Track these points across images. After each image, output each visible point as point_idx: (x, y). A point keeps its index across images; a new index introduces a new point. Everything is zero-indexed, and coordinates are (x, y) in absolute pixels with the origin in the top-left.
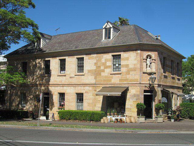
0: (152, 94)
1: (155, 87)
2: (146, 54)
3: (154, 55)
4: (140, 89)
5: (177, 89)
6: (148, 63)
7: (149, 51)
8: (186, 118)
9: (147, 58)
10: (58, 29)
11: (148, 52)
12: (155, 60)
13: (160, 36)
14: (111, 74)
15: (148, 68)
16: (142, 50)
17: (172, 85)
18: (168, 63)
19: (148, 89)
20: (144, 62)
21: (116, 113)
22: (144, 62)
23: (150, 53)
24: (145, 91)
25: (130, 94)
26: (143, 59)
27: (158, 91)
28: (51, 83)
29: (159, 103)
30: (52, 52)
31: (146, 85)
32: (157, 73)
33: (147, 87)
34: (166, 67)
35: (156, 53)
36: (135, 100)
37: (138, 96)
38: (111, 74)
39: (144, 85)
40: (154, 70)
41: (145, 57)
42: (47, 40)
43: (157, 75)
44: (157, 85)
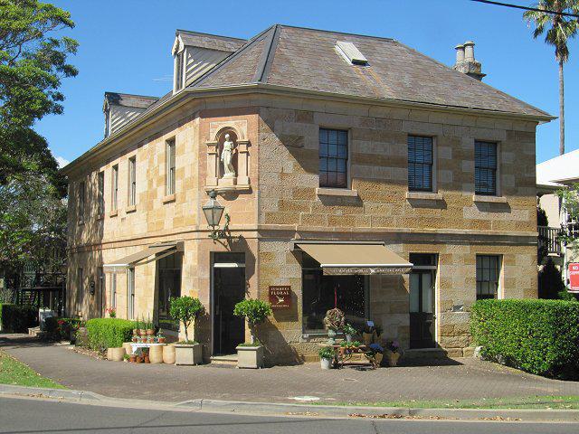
0: (243, 265)
2: (218, 124)
3: (244, 126)
5: (471, 244)
6: (227, 157)
8: (497, 362)
11: (223, 118)
13: (472, 45)
14: (165, 203)
15: (229, 175)
16: (205, 114)
17: (405, 230)
19: (223, 249)
23: (230, 122)
24: (216, 257)
26: (209, 145)
28: (106, 238)
30: (349, 140)
35: (254, 117)
38: (165, 203)
40: (243, 182)
41: (213, 139)
42: (131, 114)
44: (255, 234)
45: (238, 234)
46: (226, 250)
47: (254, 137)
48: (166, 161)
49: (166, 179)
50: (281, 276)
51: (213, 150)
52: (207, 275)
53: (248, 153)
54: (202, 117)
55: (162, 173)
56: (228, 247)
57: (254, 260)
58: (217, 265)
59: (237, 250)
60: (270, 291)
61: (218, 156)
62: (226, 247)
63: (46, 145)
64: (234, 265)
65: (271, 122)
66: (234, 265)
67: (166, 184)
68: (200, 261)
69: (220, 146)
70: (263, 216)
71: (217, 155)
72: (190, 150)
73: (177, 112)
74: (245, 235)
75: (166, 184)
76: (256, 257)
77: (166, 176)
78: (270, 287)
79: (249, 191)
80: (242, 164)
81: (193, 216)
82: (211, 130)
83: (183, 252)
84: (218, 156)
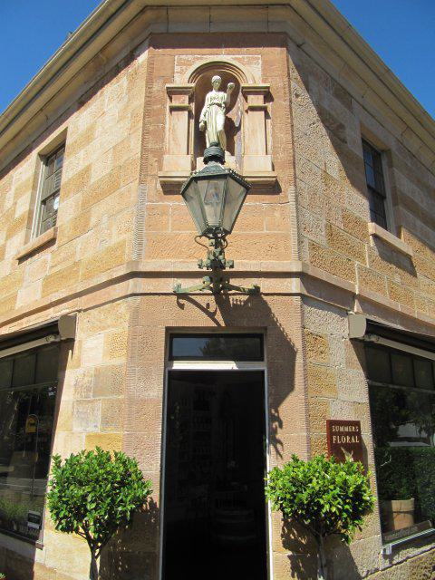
1: (275, 306)
4: (135, 320)
6: (214, 119)
7: (219, 46)
9: (206, 87)
10: (122, 272)
12: (268, 96)
14: (22, 259)
18: (400, 181)
19: (203, 321)
20: (173, 109)
21: (356, 522)
22: (173, 109)
25: (80, 371)
26: (171, 92)
27: (313, 339)
29: (336, 451)
31: (188, 285)
32: (288, 191)
33: (202, 301)
34: (395, 204)
35: (277, 54)
36: (98, 430)
37: (117, 389)
38: (22, 259)
39: (170, 285)
41: (182, 79)
43: (292, 205)
44: (294, 285)
45: (248, 284)
46: (213, 324)
47: (277, 84)
48: (34, 188)
49: (30, 218)
50: (341, 396)
51: (183, 100)
52: (155, 391)
53: (265, 109)
54: (156, 47)
55: (22, 209)
56: (219, 317)
57: (293, 353)
58: (179, 366)
59: (245, 324)
60: (330, 434)
61: (195, 116)
62: (212, 315)
63: (284, 543)
64: (230, 366)
65: (308, 71)
66: (230, 366)
67: (29, 228)
68: (135, 346)
69: (198, 98)
70: (306, 245)
71: (190, 112)
72: (141, 70)
73: (81, 78)
74: (266, 285)
75: (29, 228)
76: (298, 345)
78: (331, 423)
79: (272, 188)
80: (254, 132)
81: (121, 245)
82: (177, 69)
83: (73, 340)
84: (195, 116)
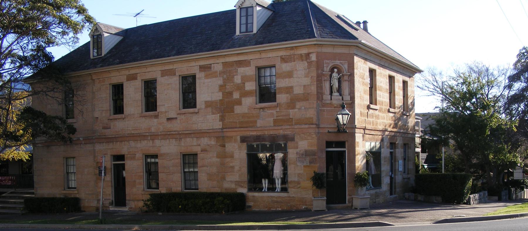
6: (336, 85)
77: (256, 90)
